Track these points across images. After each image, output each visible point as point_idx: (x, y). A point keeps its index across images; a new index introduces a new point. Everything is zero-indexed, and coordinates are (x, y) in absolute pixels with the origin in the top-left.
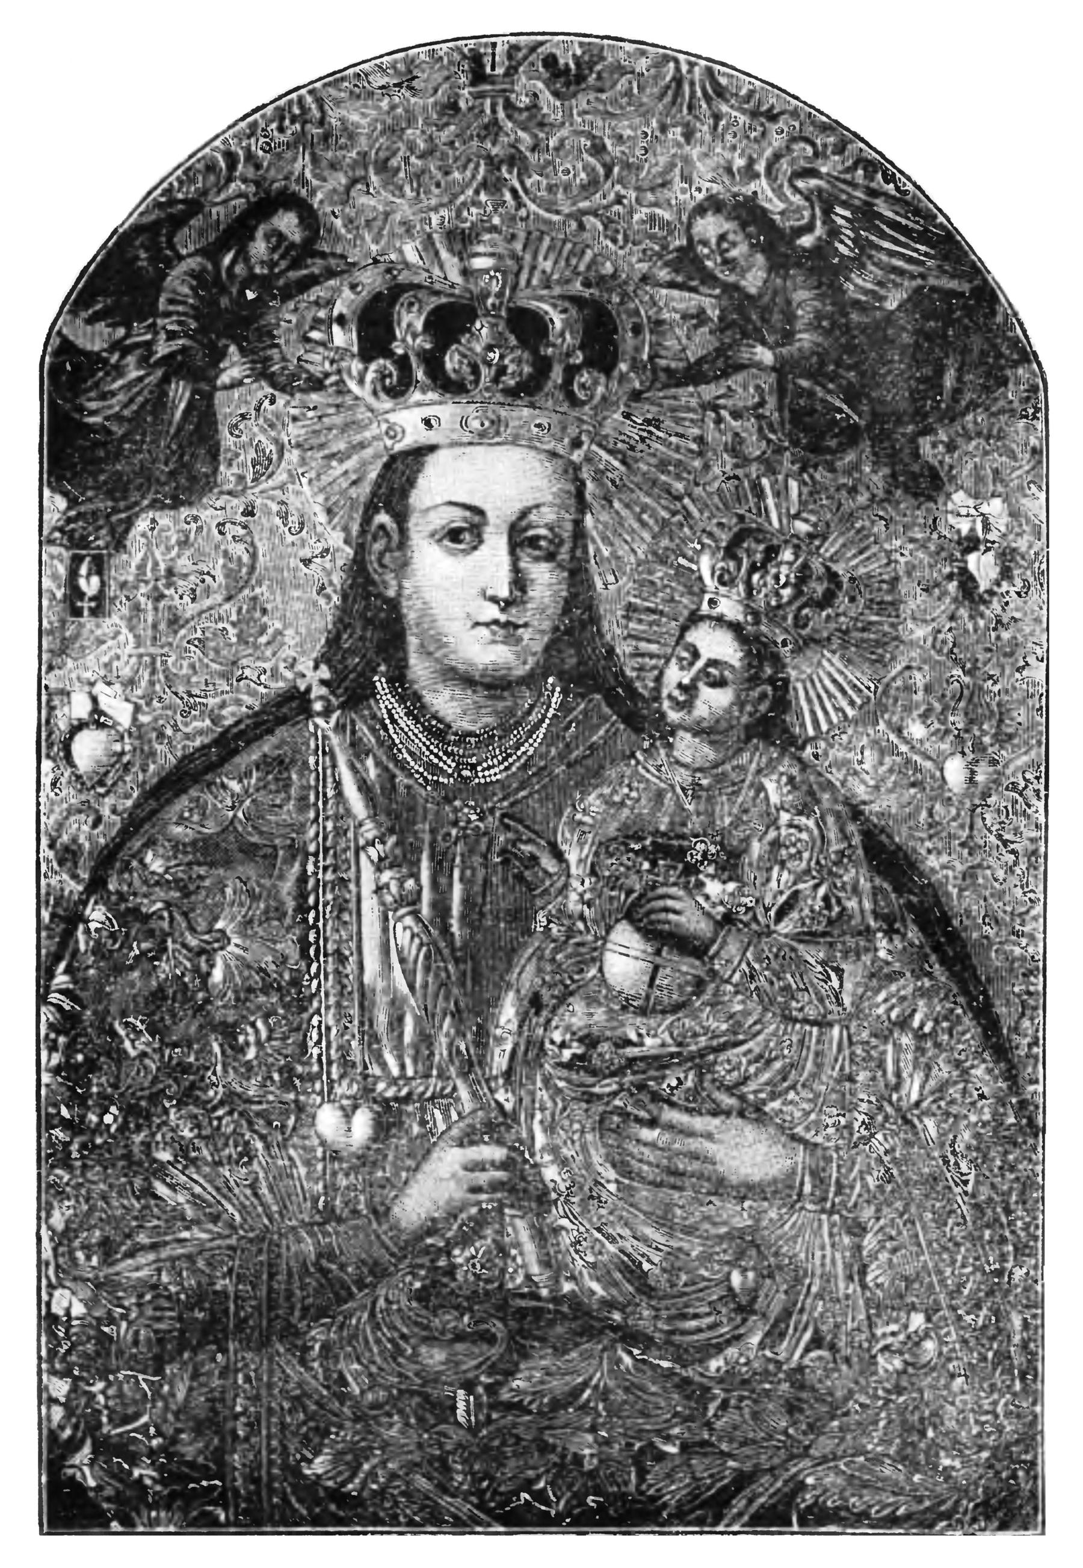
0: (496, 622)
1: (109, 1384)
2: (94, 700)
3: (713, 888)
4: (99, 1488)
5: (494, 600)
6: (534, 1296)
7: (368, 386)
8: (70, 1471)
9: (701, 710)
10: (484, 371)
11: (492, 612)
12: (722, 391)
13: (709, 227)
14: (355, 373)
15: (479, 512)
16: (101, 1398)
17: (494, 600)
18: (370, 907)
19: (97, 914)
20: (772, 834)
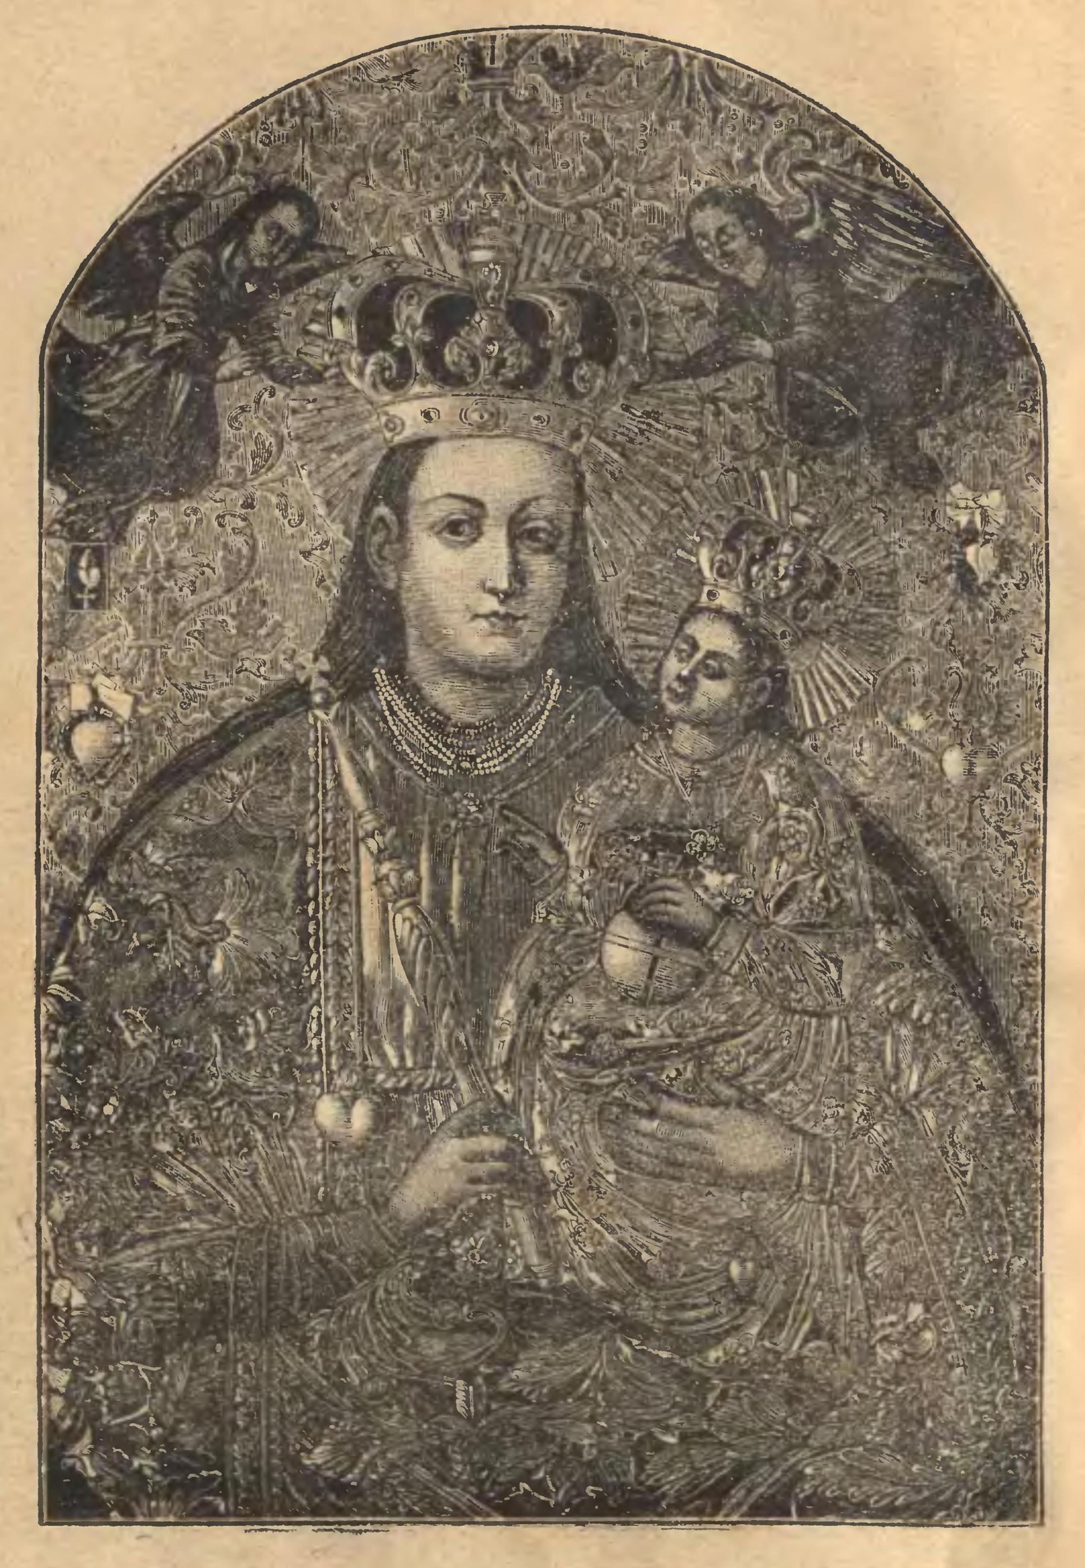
0: (495, 614)
1: (109, 1374)
2: (94, 692)
3: (712, 879)
4: (99, 1478)
5: (493, 592)
6: (535, 1287)
7: (367, 379)
8: (70, 1462)
9: (700, 701)
10: (484, 363)
11: (491, 604)
12: (721, 384)
13: (708, 219)
14: (354, 365)
15: (479, 504)
16: (101, 1389)
17: (493, 592)
18: (369, 898)
19: (96, 906)
20: (771, 826)
